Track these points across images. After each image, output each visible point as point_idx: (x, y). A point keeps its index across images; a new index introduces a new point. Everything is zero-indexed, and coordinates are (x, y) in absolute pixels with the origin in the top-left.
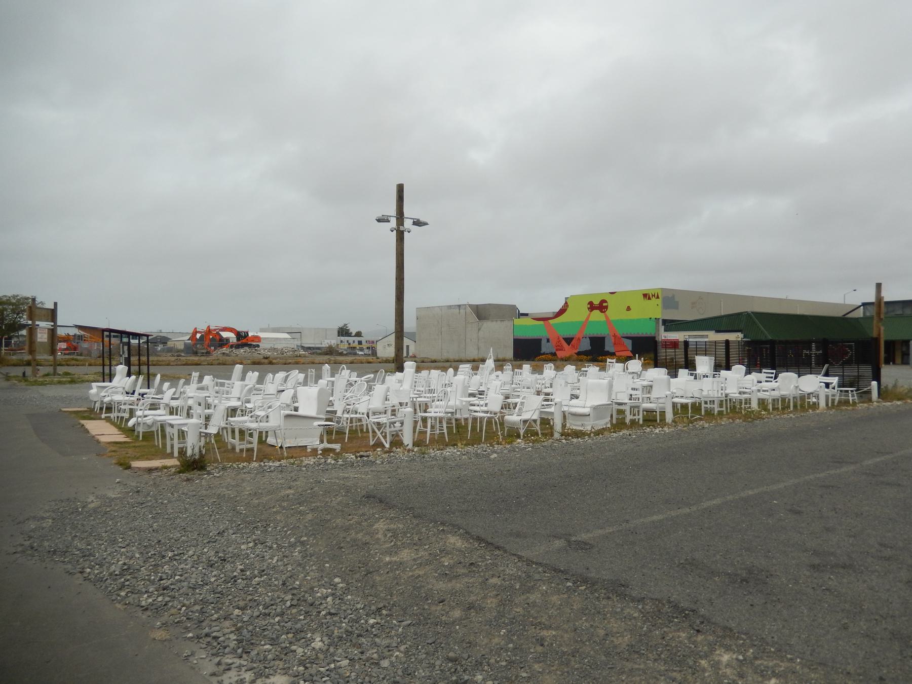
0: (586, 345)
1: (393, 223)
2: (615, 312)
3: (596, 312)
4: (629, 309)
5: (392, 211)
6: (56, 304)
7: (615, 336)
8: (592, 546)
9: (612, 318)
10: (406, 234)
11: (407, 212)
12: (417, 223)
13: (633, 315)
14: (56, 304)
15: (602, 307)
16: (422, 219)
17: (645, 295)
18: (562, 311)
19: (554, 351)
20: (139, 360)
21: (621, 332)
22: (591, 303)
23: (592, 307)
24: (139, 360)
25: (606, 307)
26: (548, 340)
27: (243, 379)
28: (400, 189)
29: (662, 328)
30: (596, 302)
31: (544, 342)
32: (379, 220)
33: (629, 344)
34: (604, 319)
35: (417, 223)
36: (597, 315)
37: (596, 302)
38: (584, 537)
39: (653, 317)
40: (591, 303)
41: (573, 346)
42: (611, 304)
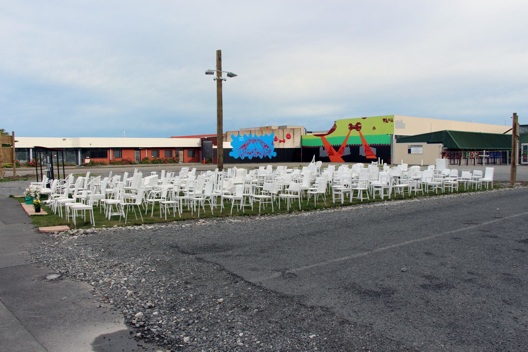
0: (347, 152)
1: (215, 76)
2: (365, 131)
3: (354, 131)
4: (374, 128)
5: (214, 68)
6: (13, 133)
7: (366, 146)
8: (296, 276)
9: (363, 135)
10: (223, 81)
11: (223, 69)
12: (231, 75)
13: (376, 132)
14: (13, 133)
15: (358, 127)
16: (234, 73)
17: (384, 120)
18: (332, 130)
19: (327, 155)
20: (15, 172)
21: (369, 143)
22: (350, 125)
23: (351, 127)
24: (15, 172)
25: (360, 127)
26: (324, 149)
27: (165, 176)
28: (219, 53)
29: (394, 140)
30: (354, 124)
31: (321, 149)
32: (207, 73)
33: (374, 150)
34: (359, 135)
35: (231, 75)
36: (354, 132)
37: (354, 124)
38: (293, 271)
39: (389, 133)
40: (350, 125)
41: (340, 152)
42: (364, 125)
